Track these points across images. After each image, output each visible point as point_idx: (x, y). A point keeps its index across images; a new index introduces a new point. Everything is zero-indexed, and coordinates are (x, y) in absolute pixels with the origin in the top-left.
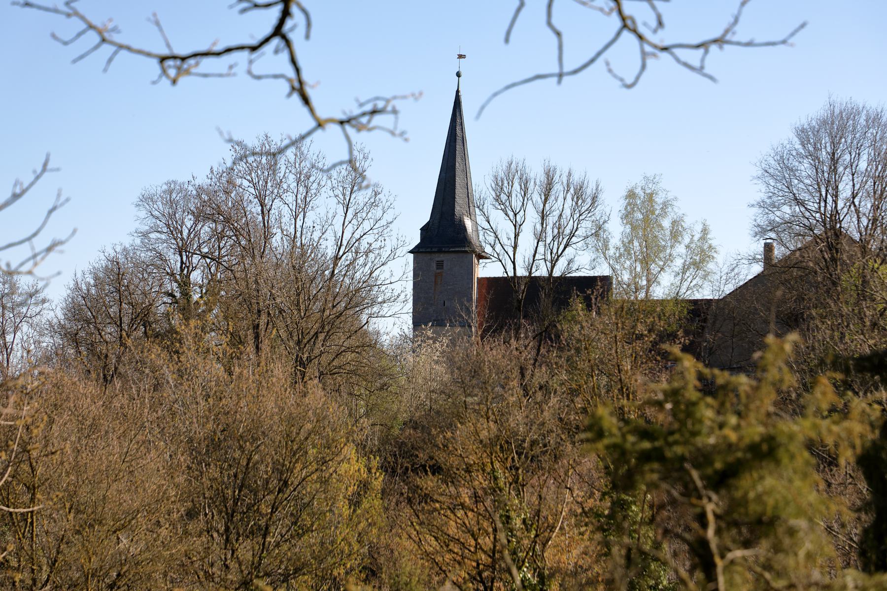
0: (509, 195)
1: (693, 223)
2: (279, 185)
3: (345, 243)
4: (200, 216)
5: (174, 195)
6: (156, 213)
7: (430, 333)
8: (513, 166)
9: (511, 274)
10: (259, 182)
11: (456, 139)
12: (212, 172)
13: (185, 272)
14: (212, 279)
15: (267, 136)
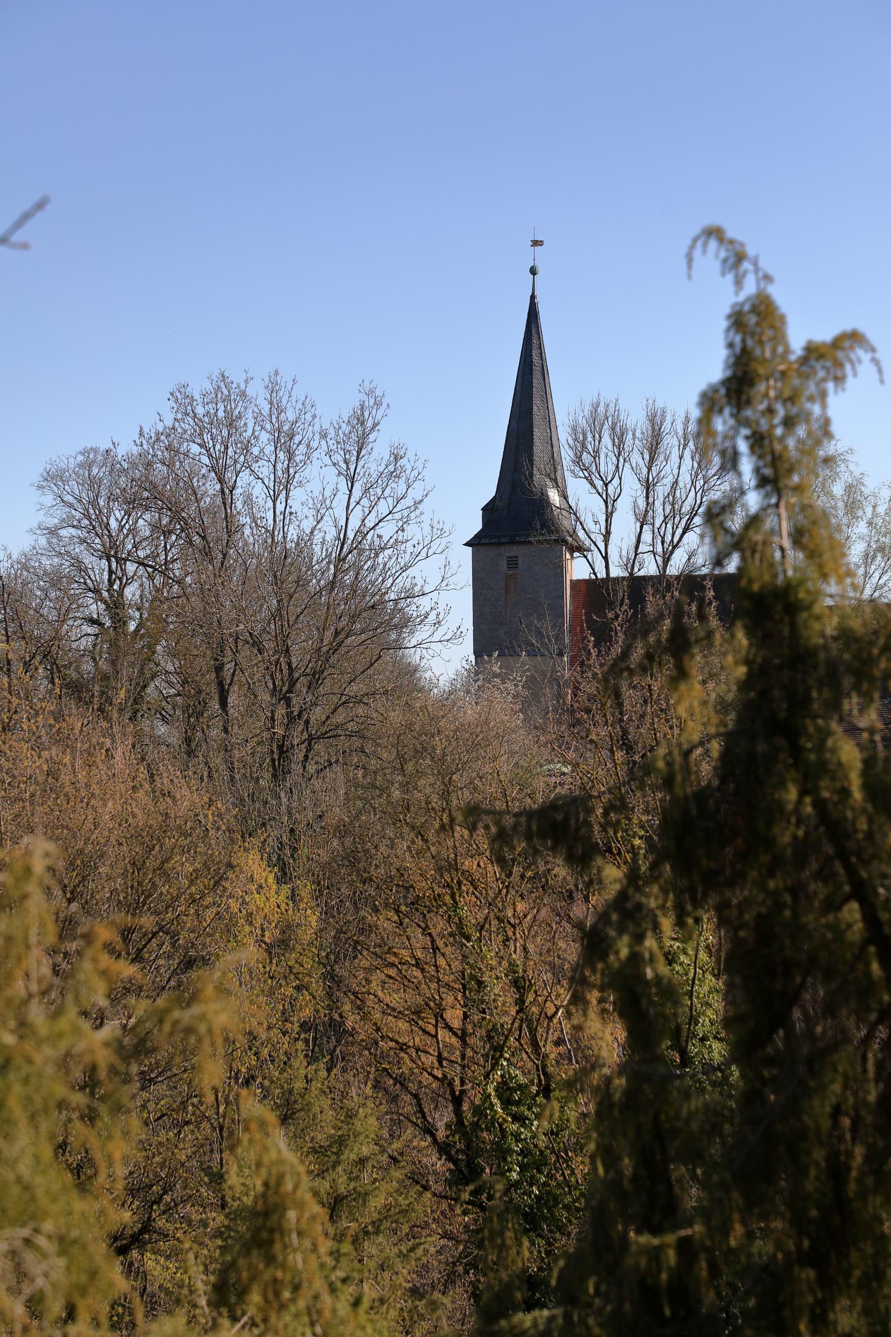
0: (596, 454)
2: (246, 448)
3: (351, 535)
4: (132, 504)
5: (95, 471)
6: (69, 498)
7: (496, 669)
8: (601, 409)
9: (602, 574)
10: (214, 446)
11: (531, 370)
12: (141, 434)
13: (116, 587)
14: (157, 599)
15: (223, 376)
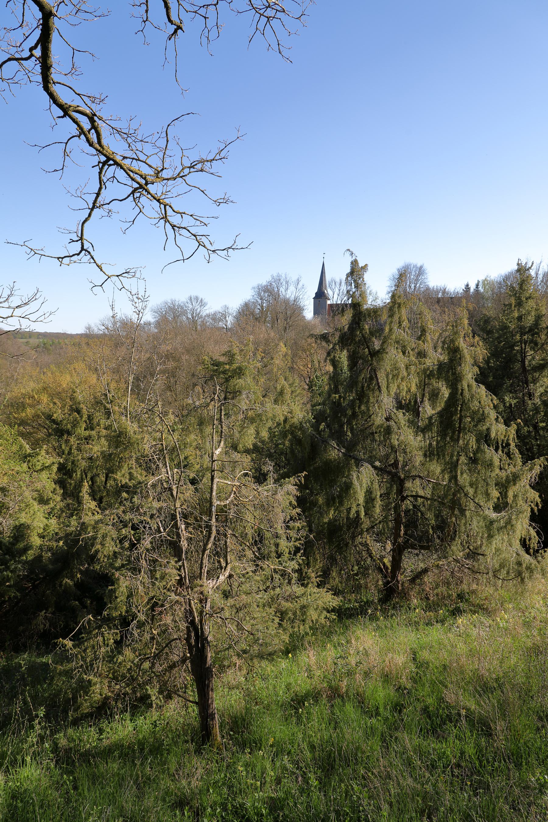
1: (374, 291)
